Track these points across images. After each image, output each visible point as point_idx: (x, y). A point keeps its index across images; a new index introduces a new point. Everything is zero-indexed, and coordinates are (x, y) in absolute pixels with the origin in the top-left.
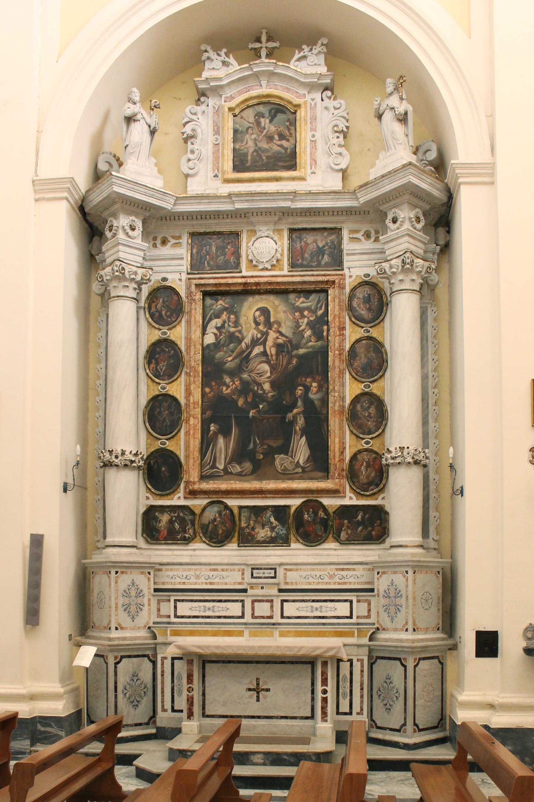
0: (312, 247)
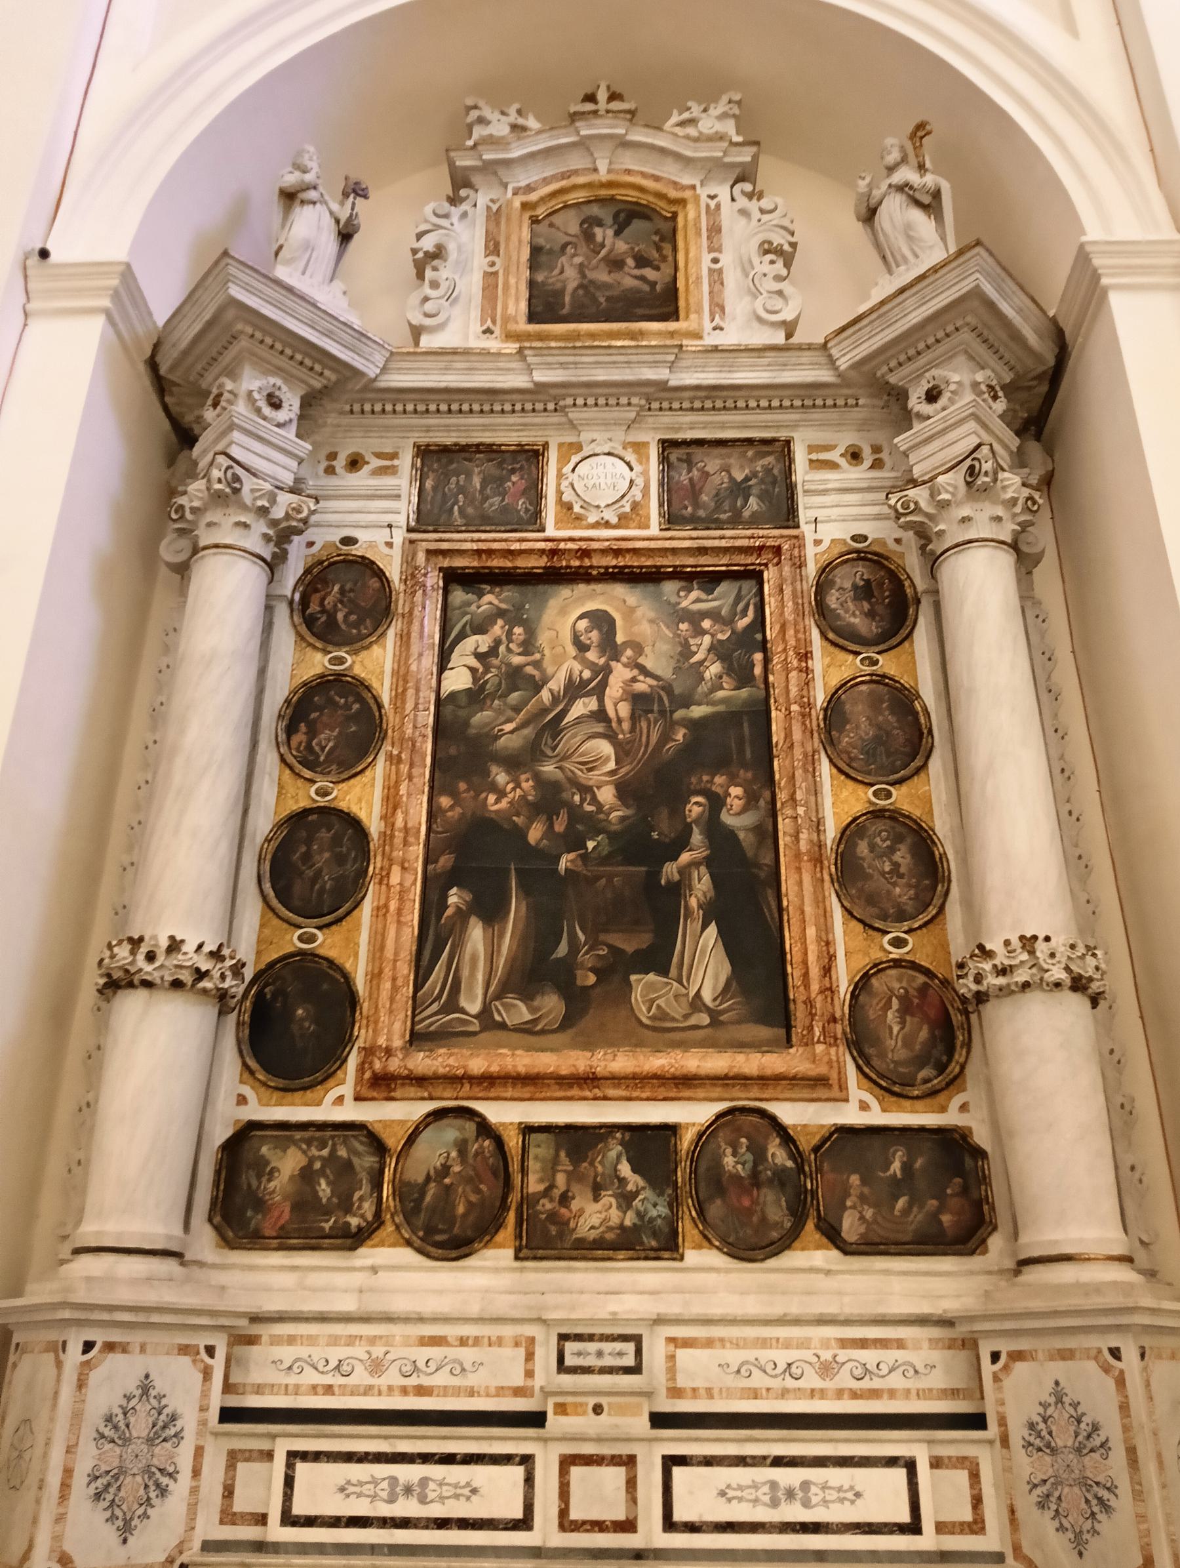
0: (719, 480)
